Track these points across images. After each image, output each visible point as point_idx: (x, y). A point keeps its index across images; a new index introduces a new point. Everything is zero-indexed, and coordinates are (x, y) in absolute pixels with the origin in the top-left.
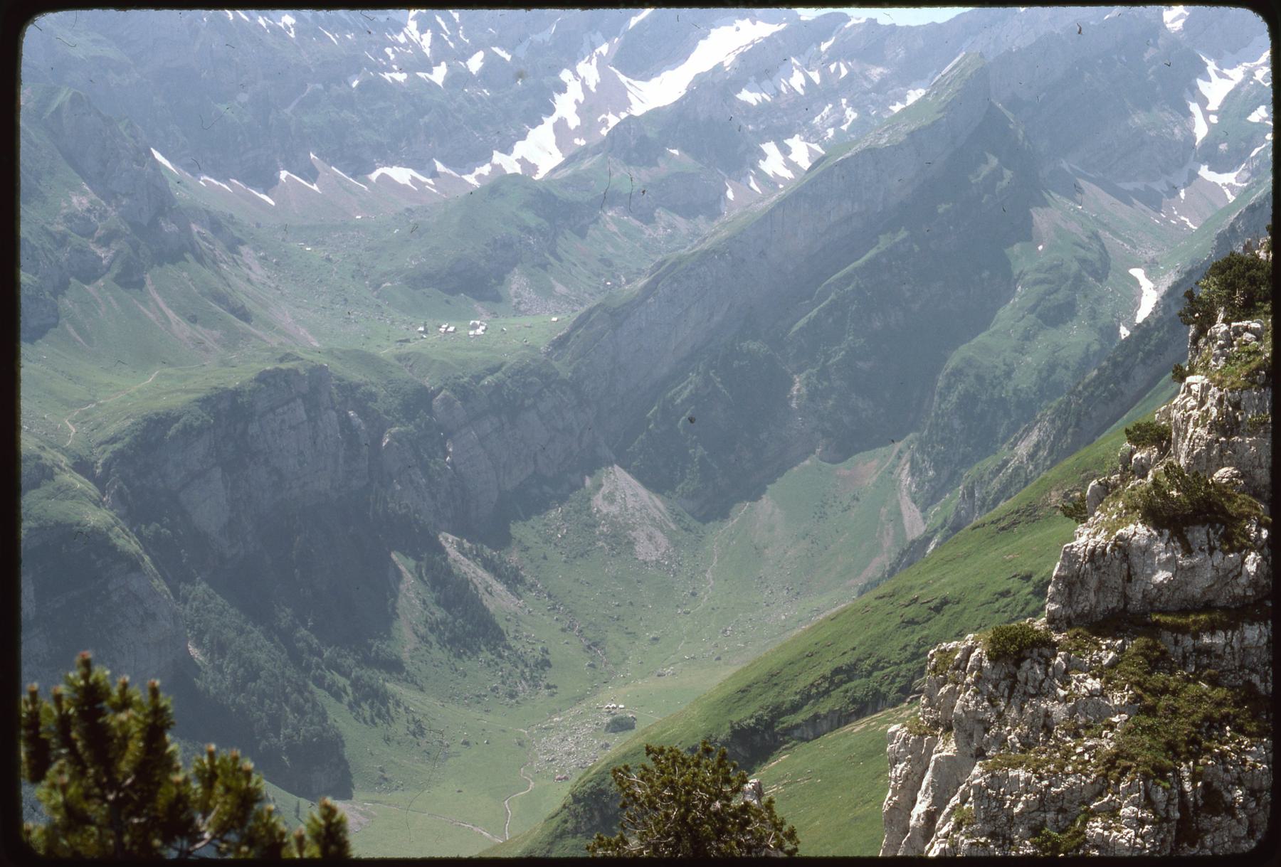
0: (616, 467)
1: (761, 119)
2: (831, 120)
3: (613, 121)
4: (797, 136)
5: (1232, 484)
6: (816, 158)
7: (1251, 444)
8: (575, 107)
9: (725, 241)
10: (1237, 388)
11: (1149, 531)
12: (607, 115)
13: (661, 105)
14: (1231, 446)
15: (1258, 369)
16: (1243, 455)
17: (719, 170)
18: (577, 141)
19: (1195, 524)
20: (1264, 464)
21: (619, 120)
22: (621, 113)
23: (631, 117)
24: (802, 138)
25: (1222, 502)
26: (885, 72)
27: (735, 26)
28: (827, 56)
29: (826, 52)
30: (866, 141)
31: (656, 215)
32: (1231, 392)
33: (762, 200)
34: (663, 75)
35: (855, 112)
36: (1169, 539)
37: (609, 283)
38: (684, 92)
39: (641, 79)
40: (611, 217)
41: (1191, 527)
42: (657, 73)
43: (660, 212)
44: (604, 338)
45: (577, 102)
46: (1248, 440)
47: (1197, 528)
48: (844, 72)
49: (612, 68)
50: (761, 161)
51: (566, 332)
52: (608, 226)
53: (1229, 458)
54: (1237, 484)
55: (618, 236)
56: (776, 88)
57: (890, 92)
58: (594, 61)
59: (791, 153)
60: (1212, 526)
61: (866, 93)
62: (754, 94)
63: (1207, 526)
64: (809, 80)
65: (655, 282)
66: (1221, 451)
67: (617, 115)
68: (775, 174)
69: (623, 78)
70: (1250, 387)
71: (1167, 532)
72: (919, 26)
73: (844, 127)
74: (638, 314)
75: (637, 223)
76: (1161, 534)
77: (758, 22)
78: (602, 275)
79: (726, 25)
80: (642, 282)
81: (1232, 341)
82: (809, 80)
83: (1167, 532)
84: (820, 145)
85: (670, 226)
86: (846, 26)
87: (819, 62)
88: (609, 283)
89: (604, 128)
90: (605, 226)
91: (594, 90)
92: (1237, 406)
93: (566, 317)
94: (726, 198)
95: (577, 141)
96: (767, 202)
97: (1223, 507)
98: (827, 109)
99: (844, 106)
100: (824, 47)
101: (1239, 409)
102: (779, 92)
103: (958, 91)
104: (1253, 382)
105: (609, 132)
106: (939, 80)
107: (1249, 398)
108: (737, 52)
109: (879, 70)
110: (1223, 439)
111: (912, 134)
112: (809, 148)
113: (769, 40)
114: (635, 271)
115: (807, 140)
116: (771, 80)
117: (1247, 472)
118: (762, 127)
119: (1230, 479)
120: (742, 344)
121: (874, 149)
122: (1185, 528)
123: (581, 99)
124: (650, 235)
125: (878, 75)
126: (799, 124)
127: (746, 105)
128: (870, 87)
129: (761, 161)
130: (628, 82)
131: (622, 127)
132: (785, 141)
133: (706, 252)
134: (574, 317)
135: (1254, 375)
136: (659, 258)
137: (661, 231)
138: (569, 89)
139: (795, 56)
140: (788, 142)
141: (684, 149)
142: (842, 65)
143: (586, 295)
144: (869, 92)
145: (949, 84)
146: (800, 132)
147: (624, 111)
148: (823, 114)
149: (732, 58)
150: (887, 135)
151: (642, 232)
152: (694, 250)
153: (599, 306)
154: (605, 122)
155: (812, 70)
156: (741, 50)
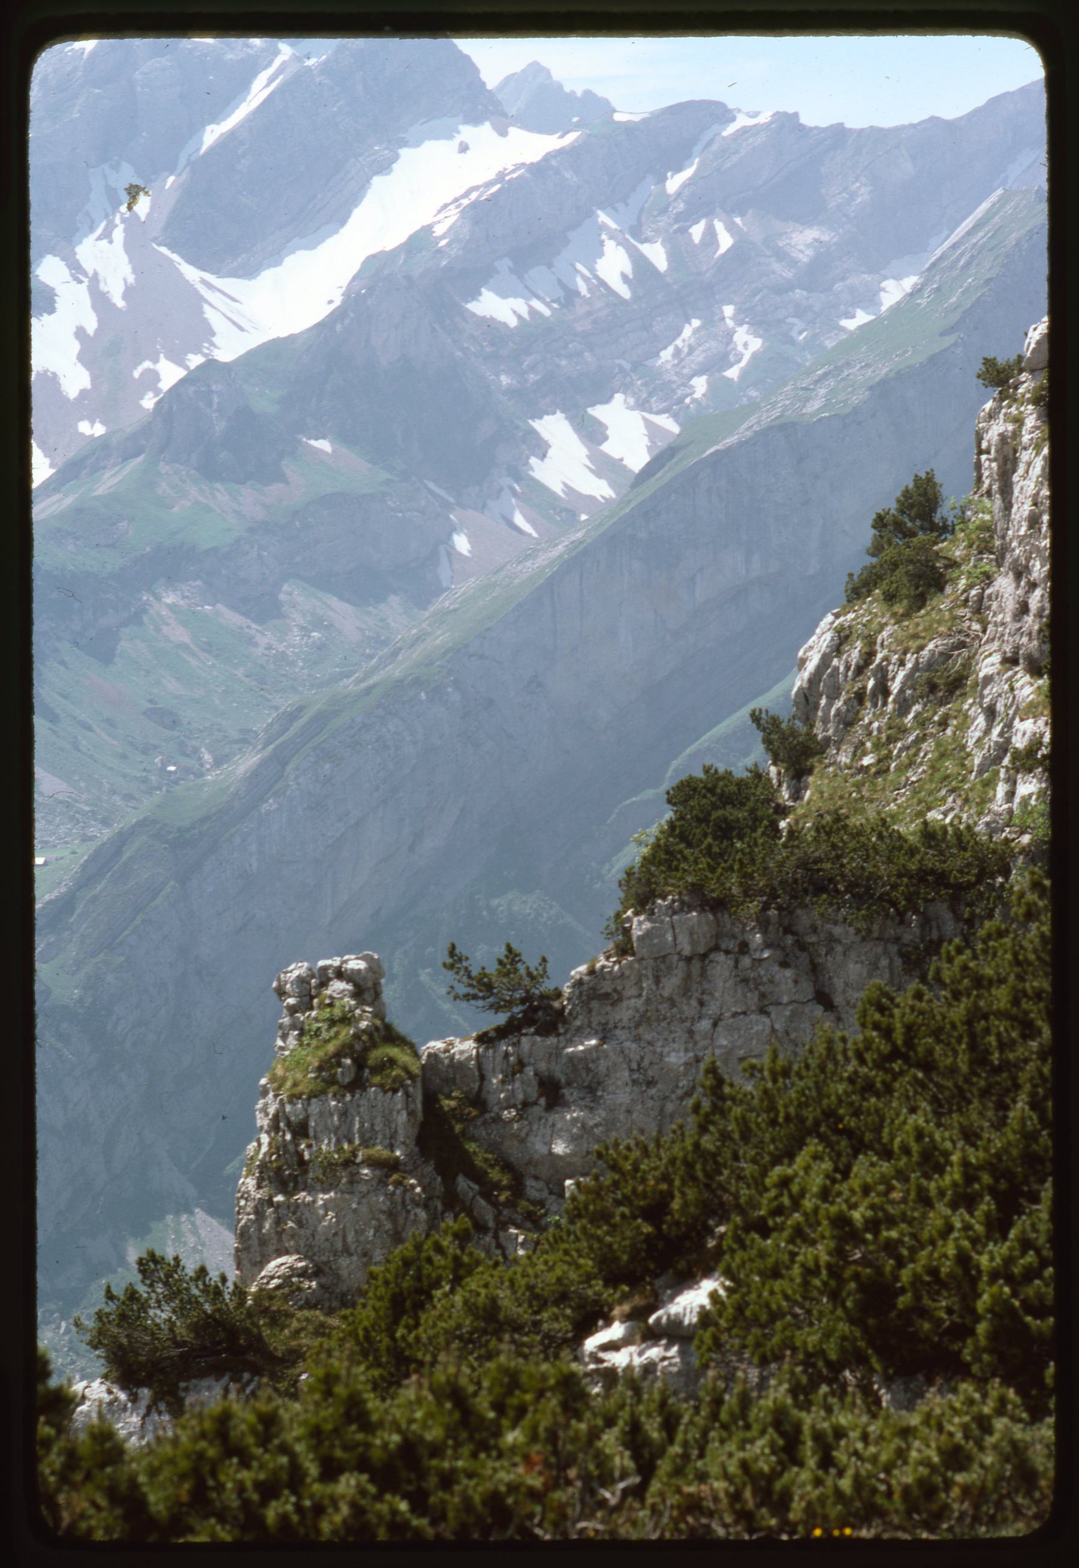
0: (200, 1214)
1: (527, 361)
2: (699, 357)
3: (170, 374)
4: (619, 397)
5: (286, 1290)
6: (662, 444)
7: (326, 1207)
8: (76, 347)
9: (444, 655)
10: (301, 1094)
11: (110, 1392)
12: (156, 361)
13: (284, 334)
14: (294, 1213)
15: (338, 1055)
16: (315, 1231)
17: (431, 485)
18: (84, 427)
19: (203, 1374)
20: (353, 1247)
21: (181, 373)
22: (190, 356)
23: (211, 364)
24: (631, 401)
25: (257, 1326)
26: (825, 238)
27: (458, 139)
28: (682, 206)
29: (679, 194)
30: (774, 405)
31: (282, 597)
32: (290, 1102)
33: (530, 555)
34: (289, 261)
35: (757, 335)
36: (149, 1409)
37: (172, 768)
38: (338, 301)
39: (234, 274)
40: (172, 607)
41: (194, 1381)
42: (275, 258)
43: (292, 593)
44: (159, 900)
45: (80, 333)
46: (322, 1198)
47: (205, 1383)
48: (725, 241)
49: (164, 250)
50: (533, 461)
51: (63, 890)
52: (165, 630)
53: (293, 1236)
54: (299, 1289)
55: (193, 655)
56: (560, 283)
57: (838, 286)
58: (118, 234)
59: (606, 438)
60: (235, 1379)
61: (783, 289)
62: (511, 300)
63: (226, 1378)
64: (641, 263)
65: (279, 760)
66: (278, 1221)
67: (180, 362)
68: (569, 489)
69: (191, 273)
70: (324, 1092)
71: (145, 1393)
72: (902, 128)
73: (733, 373)
74: (237, 840)
75: (234, 619)
76: (134, 1398)
77: (512, 130)
78: (155, 747)
79: (437, 138)
80: (246, 763)
81: (312, 998)
82: (641, 263)
83: (145, 1393)
84: (675, 416)
85: (318, 623)
86: (725, 134)
87: (663, 221)
88: (172, 768)
89: (150, 394)
90: (158, 630)
91: (120, 303)
92: (301, 1130)
93: (66, 853)
94: (452, 553)
95: (84, 427)
96: (542, 560)
97: (259, 1338)
98: (687, 332)
99: (730, 323)
100: (674, 183)
101: (306, 1135)
102: (570, 295)
103: (988, 281)
104: (332, 1081)
105: (158, 404)
106: (941, 258)
107: (321, 1114)
108: (465, 202)
109: (812, 234)
110: (280, 1198)
111: (882, 389)
112: (648, 424)
113: (539, 170)
114: (234, 734)
115: (642, 405)
116: (550, 266)
117: (325, 1263)
118: (532, 377)
119: (286, 1279)
120: (495, 902)
121: (793, 425)
122: (182, 1385)
123: (91, 324)
124: (269, 647)
125: (808, 246)
126: (622, 369)
127: (490, 325)
128: (788, 274)
129: (533, 461)
130: (204, 282)
131: (192, 389)
132: (590, 410)
133: (399, 685)
134: (85, 852)
135: (332, 1067)
136: (287, 703)
137: (295, 636)
138: (60, 303)
139: (608, 205)
140: (599, 412)
141: (344, 437)
142: (719, 226)
143: (117, 799)
144: (790, 287)
145: (968, 264)
146: (625, 388)
147: (197, 350)
148: (679, 342)
149: (453, 215)
150: (822, 391)
151: (251, 642)
152: (371, 682)
153: (142, 824)
154: (153, 377)
155: (646, 240)
156: (474, 196)
